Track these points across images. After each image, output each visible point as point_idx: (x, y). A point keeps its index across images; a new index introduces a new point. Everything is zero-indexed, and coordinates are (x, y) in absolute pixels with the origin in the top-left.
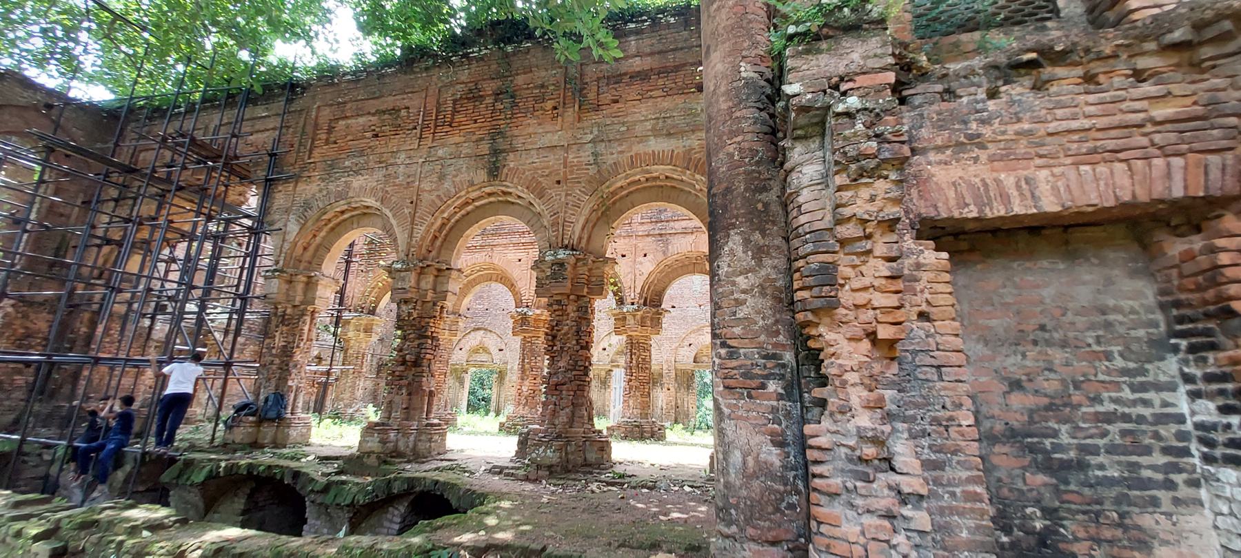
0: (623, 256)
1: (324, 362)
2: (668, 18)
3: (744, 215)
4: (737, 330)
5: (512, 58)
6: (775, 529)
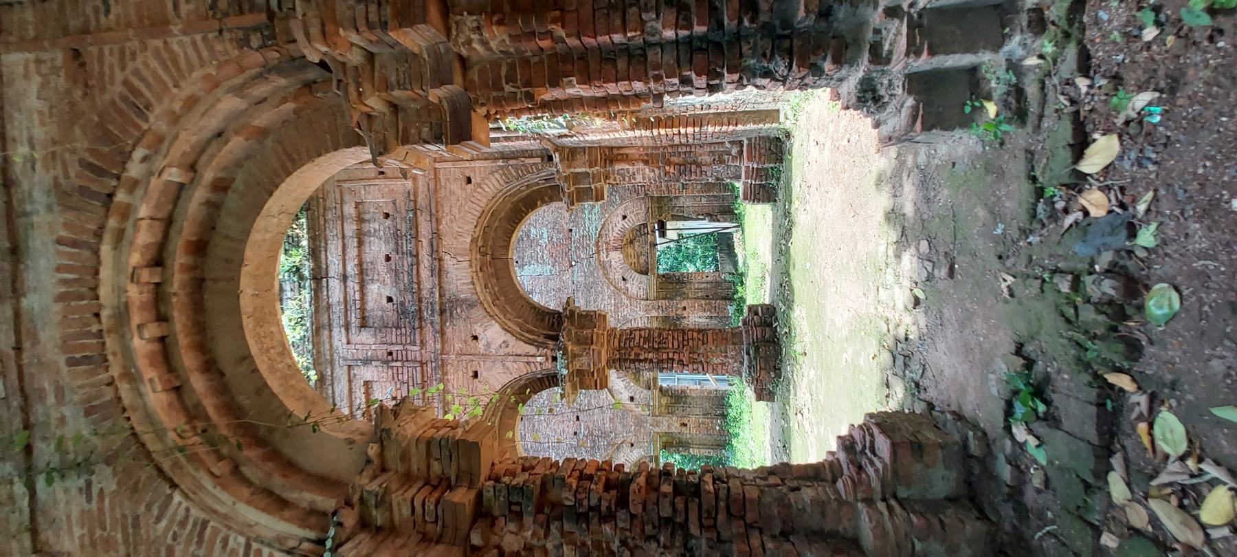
0: (476, 375)
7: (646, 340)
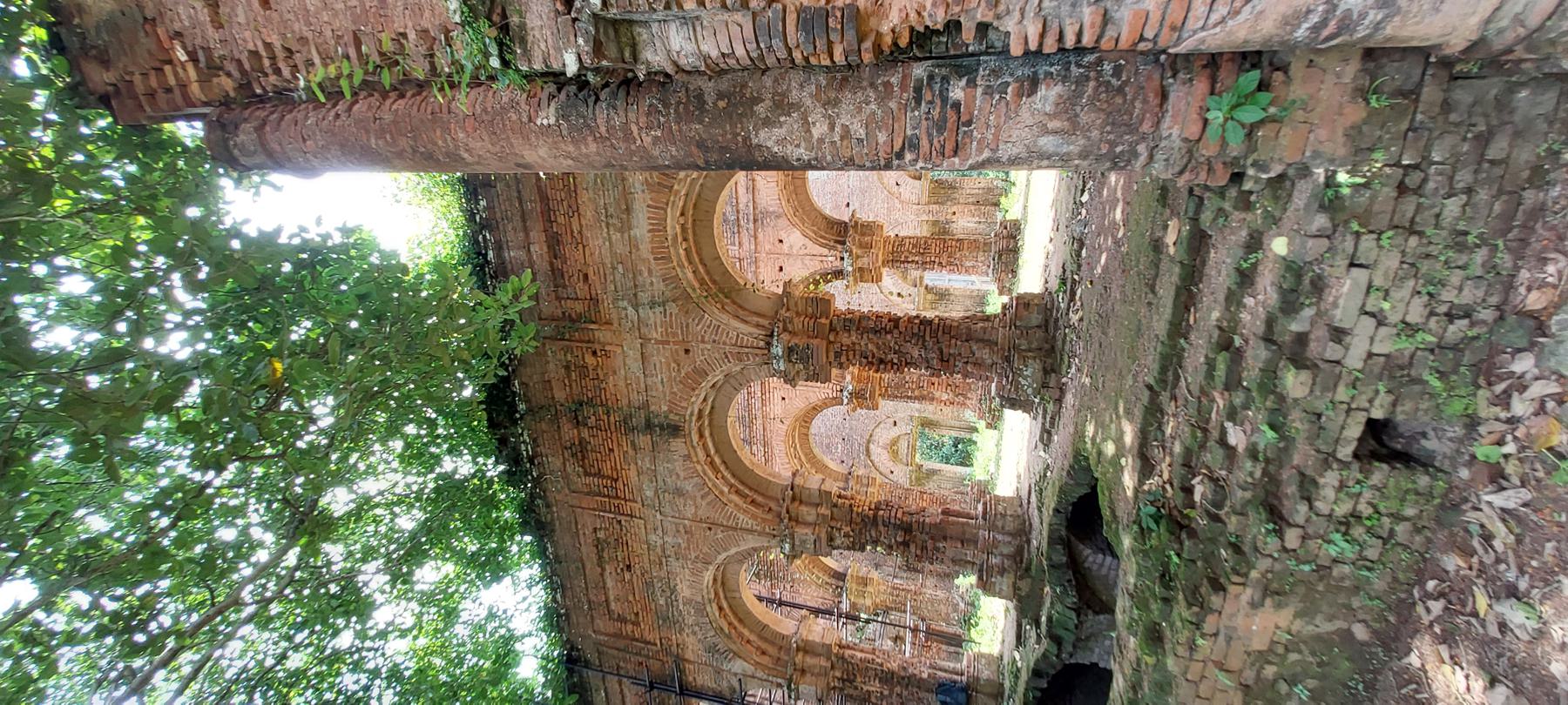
0: (781, 269)
1: (902, 634)
2: (481, 208)
3: (734, 126)
4: (882, 137)
5: (534, 404)
7: (914, 246)
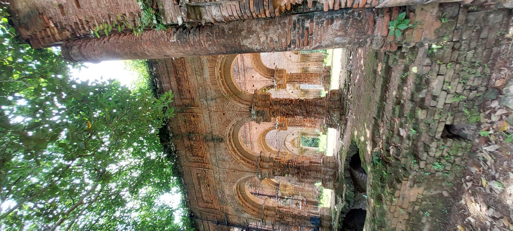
0: (253, 86)
3: (235, 39)
4: (283, 41)
6: (369, 22)
